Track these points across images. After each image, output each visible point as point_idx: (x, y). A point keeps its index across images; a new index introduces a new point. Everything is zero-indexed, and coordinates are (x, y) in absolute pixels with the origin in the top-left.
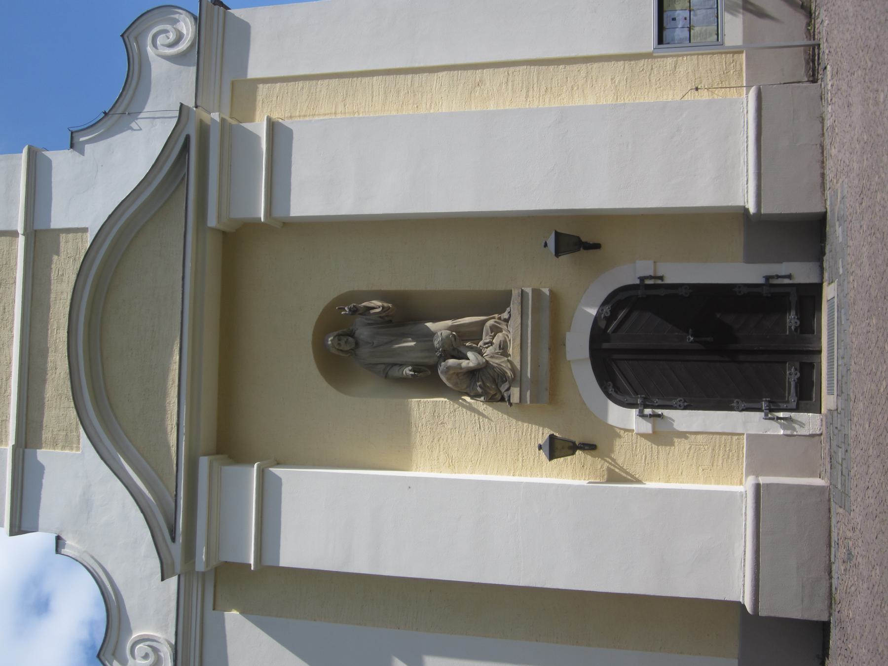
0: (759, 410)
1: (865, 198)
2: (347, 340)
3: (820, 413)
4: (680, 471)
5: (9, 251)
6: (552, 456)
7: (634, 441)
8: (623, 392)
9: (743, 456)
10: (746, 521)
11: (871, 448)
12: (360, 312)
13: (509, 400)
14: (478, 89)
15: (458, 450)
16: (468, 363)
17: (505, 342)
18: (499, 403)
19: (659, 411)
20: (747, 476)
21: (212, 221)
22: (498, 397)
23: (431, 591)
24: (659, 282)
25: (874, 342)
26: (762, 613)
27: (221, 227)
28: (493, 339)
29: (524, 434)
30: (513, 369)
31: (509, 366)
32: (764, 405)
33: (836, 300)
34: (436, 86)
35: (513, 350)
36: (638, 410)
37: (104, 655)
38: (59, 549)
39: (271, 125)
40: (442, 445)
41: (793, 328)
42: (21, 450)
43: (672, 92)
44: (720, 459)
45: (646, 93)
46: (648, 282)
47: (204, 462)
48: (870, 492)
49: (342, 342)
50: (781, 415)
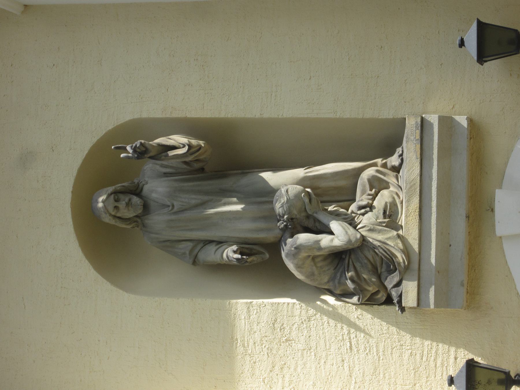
16: (332, 240)
18: (383, 307)
22: (382, 296)
28: (374, 199)
31: (401, 245)
49: (122, 205)
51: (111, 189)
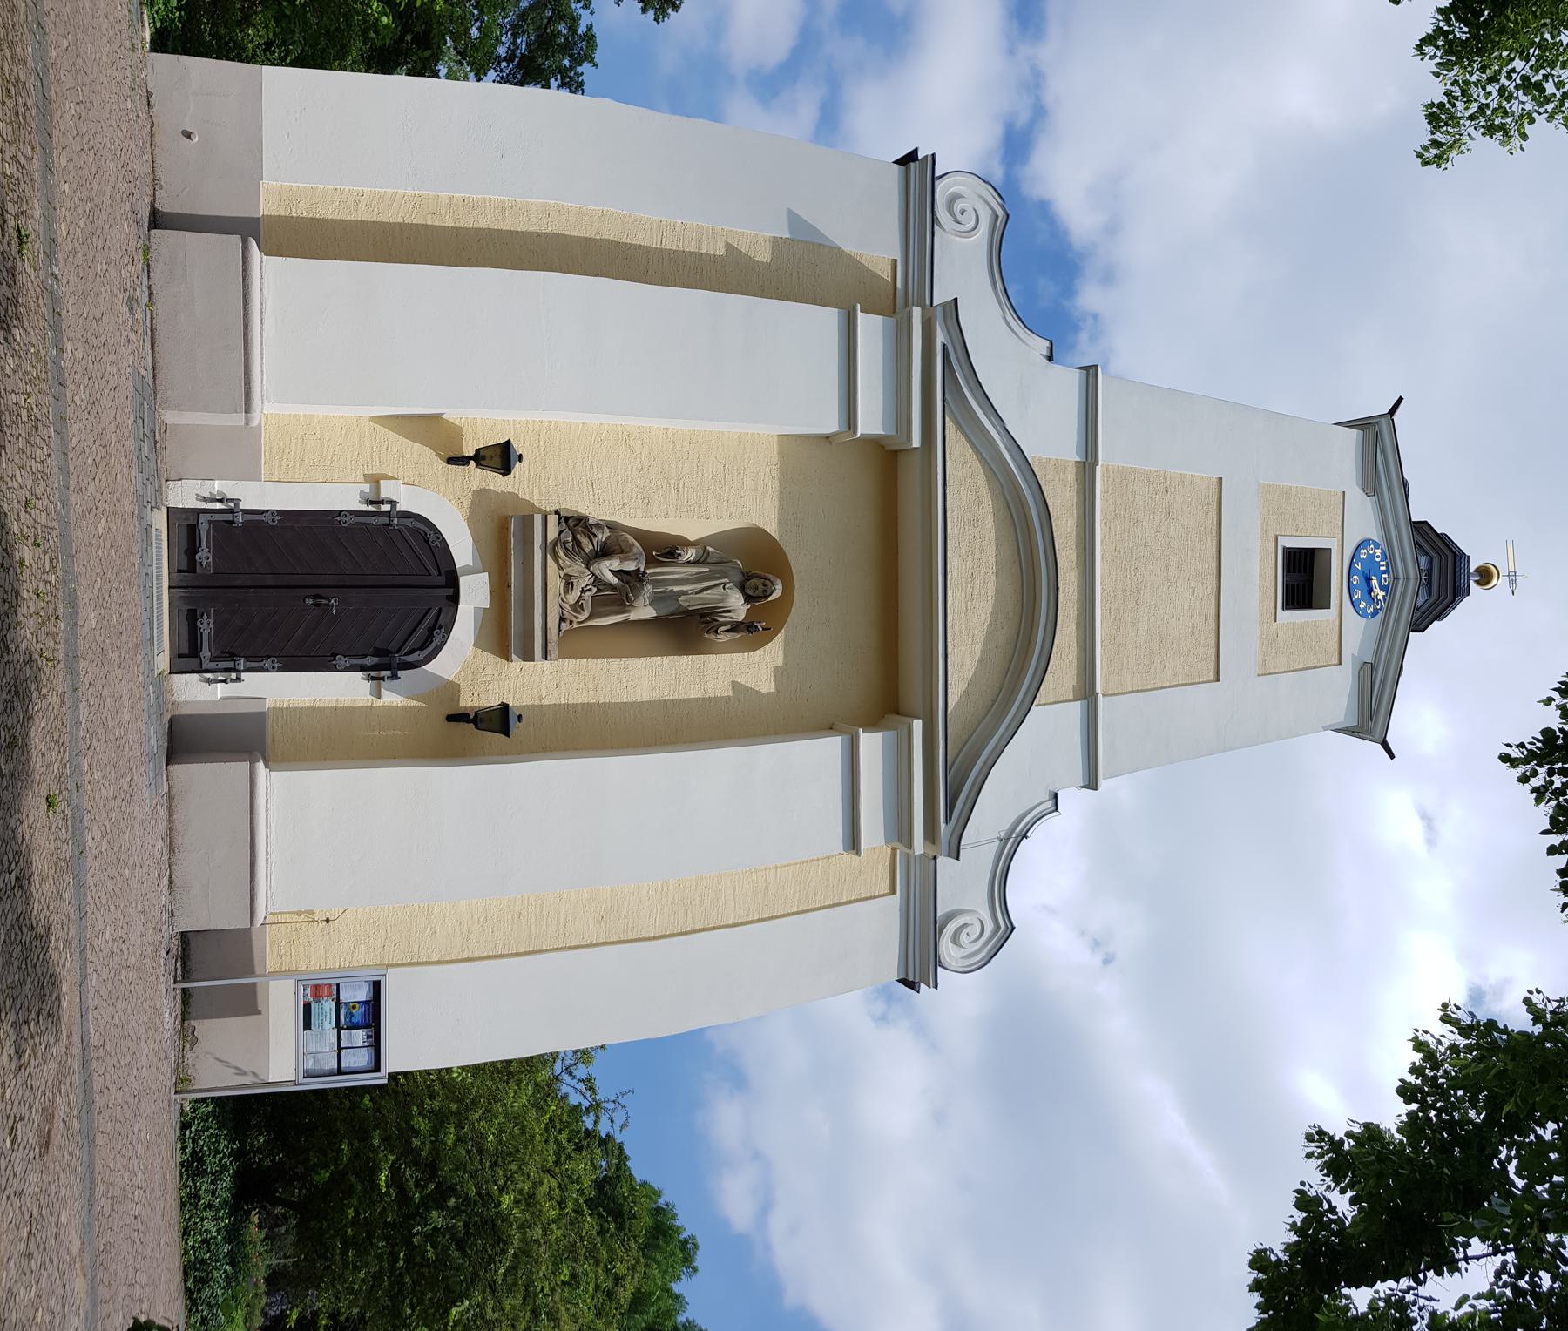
0: (246, 512)
1: (127, 788)
3: (168, 508)
4: (343, 432)
6: (507, 445)
7: (401, 469)
8: (415, 532)
9: (265, 452)
10: (262, 364)
11: (113, 443)
13: (560, 518)
14: (603, 913)
15: (618, 456)
16: (611, 565)
17: (566, 592)
19: (371, 508)
20: (260, 424)
21: (917, 725)
24: (373, 673)
25: (114, 589)
26: (238, 238)
28: (580, 597)
29: (538, 476)
30: (556, 558)
31: (561, 561)
32: (240, 518)
33: (156, 654)
34: (657, 913)
35: (555, 584)
36: (398, 510)
40: (638, 462)
41: (205, 617)
42: (1089, 460)
43: (359, 916)
44: (293, 448)
45: (391, 914)
46: (388, 673)
47: (916, 442)
48: (112, 383)
49: (761, 588)
50: (218, 506)
51: (770, 599)
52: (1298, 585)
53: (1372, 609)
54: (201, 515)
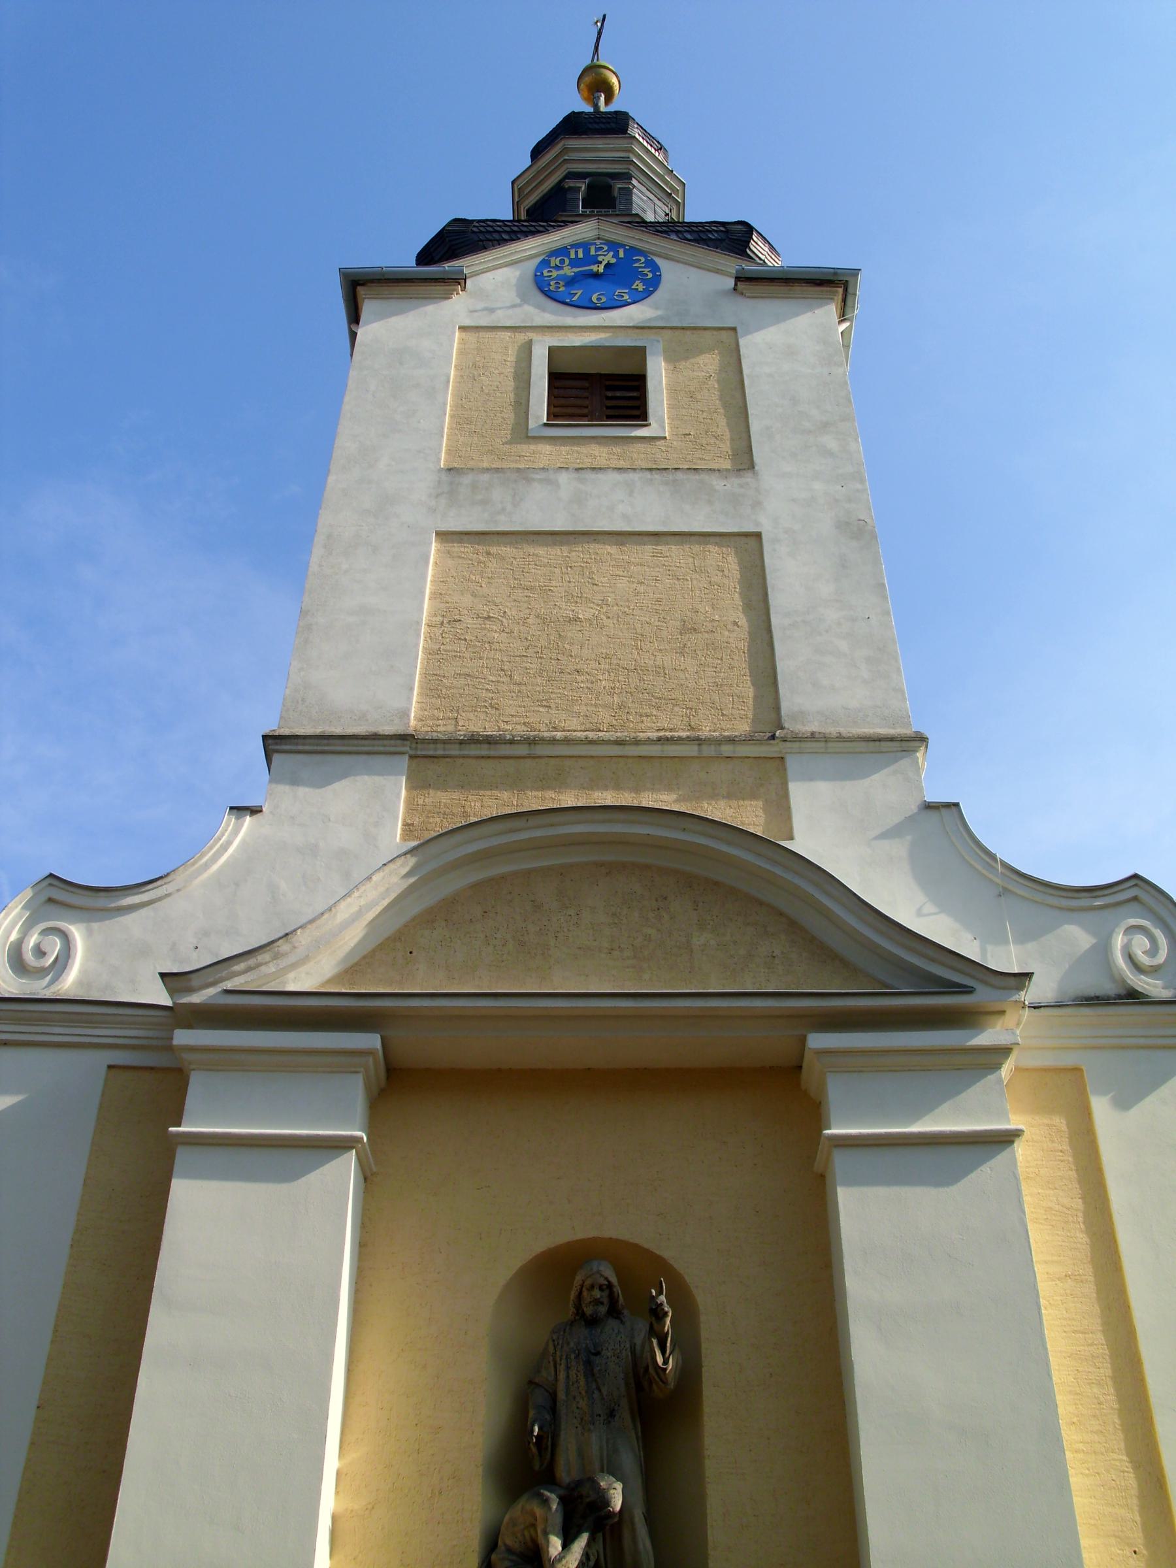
2: (602, 1303)
5: (747, 718)
12: (655, 1325)
21: (818, 1041)
23: (104, 1472)
27: (808, 1056)
37: (50, 885)
38: (235, 811)
39: (1008, 1139)
47: (371, 1041)
49: (597, 1294)
52: (608, 408)
53: (646, 271)
54: (530, 435)
